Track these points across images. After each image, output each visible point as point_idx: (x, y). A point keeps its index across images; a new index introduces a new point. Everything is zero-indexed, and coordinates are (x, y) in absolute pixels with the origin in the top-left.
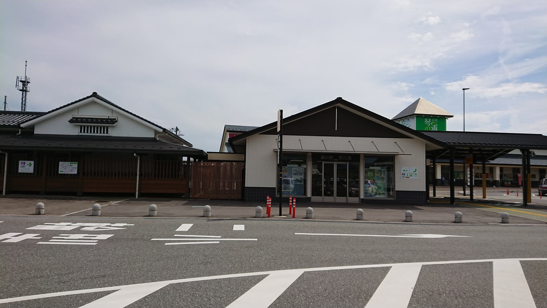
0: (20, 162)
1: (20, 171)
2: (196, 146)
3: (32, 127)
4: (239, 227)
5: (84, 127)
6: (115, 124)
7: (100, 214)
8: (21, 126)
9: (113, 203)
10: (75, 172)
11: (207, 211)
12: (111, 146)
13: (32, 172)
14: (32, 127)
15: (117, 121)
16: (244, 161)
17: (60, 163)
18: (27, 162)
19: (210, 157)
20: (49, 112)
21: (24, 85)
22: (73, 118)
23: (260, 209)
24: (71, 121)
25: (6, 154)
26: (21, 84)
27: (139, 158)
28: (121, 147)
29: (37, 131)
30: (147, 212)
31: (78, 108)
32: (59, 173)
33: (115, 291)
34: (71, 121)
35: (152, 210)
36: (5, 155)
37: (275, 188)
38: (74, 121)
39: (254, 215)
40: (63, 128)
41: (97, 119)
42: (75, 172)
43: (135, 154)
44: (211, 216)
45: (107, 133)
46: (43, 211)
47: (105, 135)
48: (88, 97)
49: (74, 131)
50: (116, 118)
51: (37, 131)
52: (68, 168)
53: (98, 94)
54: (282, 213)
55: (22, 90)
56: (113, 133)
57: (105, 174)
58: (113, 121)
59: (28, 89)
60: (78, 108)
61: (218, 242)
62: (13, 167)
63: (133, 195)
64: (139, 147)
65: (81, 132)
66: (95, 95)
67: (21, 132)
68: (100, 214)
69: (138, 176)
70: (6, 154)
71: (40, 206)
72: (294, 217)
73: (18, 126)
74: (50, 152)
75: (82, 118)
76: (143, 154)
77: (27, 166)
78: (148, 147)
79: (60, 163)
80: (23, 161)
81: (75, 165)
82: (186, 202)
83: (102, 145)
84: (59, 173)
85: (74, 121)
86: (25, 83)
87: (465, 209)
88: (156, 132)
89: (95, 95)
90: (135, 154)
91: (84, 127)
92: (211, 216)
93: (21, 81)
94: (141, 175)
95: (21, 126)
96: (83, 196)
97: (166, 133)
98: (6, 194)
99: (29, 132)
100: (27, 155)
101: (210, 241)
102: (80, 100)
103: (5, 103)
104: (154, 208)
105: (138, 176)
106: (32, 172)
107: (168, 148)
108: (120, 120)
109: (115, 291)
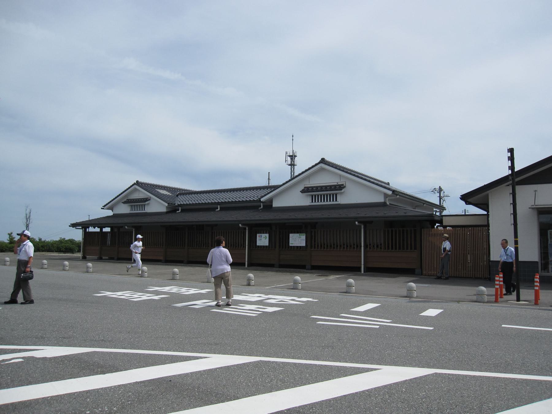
0: (258, 235)
1: (258, 244)
2: (471, 206)
3: (271, 201)
4: (432, 312)
5: (330, 195)
6: (343, 191)
7: (300, 287)
8: (262, 200)
9: (332, 277)
10: (304, 244)
11: (410, 290)
12: (343, 214)
13: (268, 245)
14: (271, 201)
15: (345, 187)
16: (488, 226)
17: (291, 235)
18: (263, 235)
19: (446, 222)
20: (284, 184)
21: (292, 159)
22: (305, 188)
23: (482, 291)
24: (303, 191)
25: (247, 228)
26: (289, 159)
27: (362, 227)
28: (344, 216)
29: (276, 204)
30: (405, 293)
31: (308, 177)
32: (290, 245)
33: (206, 357)
34: (303, 191)
35: (349, 286)
36: (245, 229)
37: (537, 262)
38: (306, 190)
39: (405, 294)
40: (296, 199)
41: (331, 186)
42: (304, 244)
43: (357, 223)
44: (417, 297)
45: (336, 200)
46: (253, 283)
47: (335, 203)
48: (316, 165)
49: (304, 201)
50: (344, 183)
51: (276, 204)
52: (297, 240)
53: (327, 159)
54: (521, 298)
55: (291, 165)
56: (343, 200)
57: (331, 246)
58: (340, 187)
59: (296, 163)
60: (308, 177)
61: (378, 327)
62: (253, 240)
63: (358, 269)
64: (363, 213)
65: (312, 202)
66: (323, 161)
67: (263, 206)
68: (300, 287)
69: (362, 248)
70: (247, 228)
71: (249, 277)
72: (536, 303)
73: (259, 200)
74: (282, 225)
75: (312, 187)
76: (367, 223)
77: (263, 239)
78: (381, 213)
79: (291, 235)
80: (260, 234)
81: (303, 237)
82: (414, 279)
83: (334, 214)
84: (290, 245)
85: (306, 190)
86: (293, 157)
87: (258, 273)
88: (386, 195)
89: (323, 161)
90: (357, 223)
91: (330, 195)
92: (417, 297)
93: (289, 156)
94: (366, 246)
95: (262, 200)
96: (311, 269)
97: (397, 195)
98: (248, 266)
99: (268, 206)
100: (297, 228)
101: (366, 324)
102: (310, 169)
103: (269, 179)
104: (351, 283)
105: (362, 248)
106: (268, 245)
107: (401, 213)
108: (349, 185)
109: (206, 357)
